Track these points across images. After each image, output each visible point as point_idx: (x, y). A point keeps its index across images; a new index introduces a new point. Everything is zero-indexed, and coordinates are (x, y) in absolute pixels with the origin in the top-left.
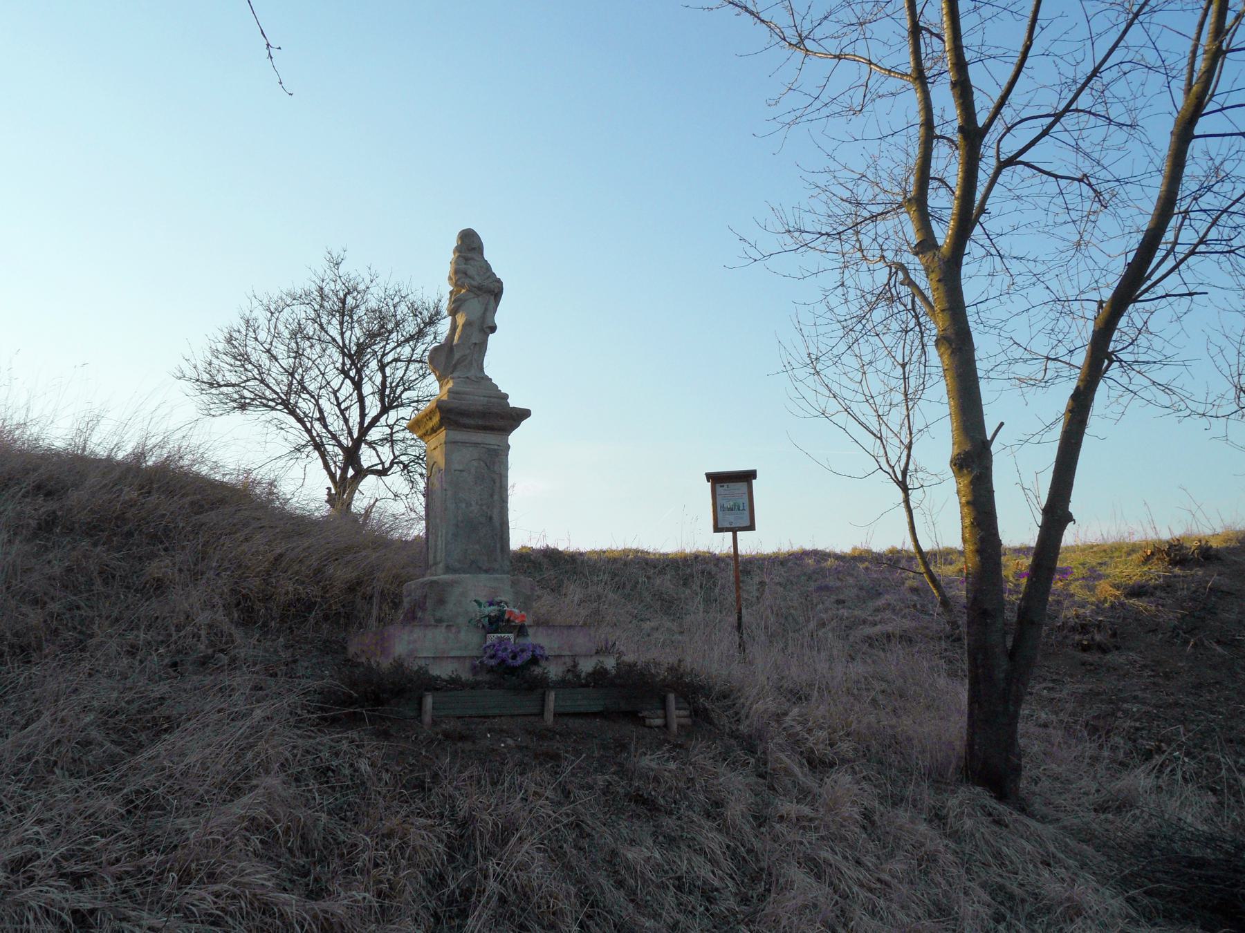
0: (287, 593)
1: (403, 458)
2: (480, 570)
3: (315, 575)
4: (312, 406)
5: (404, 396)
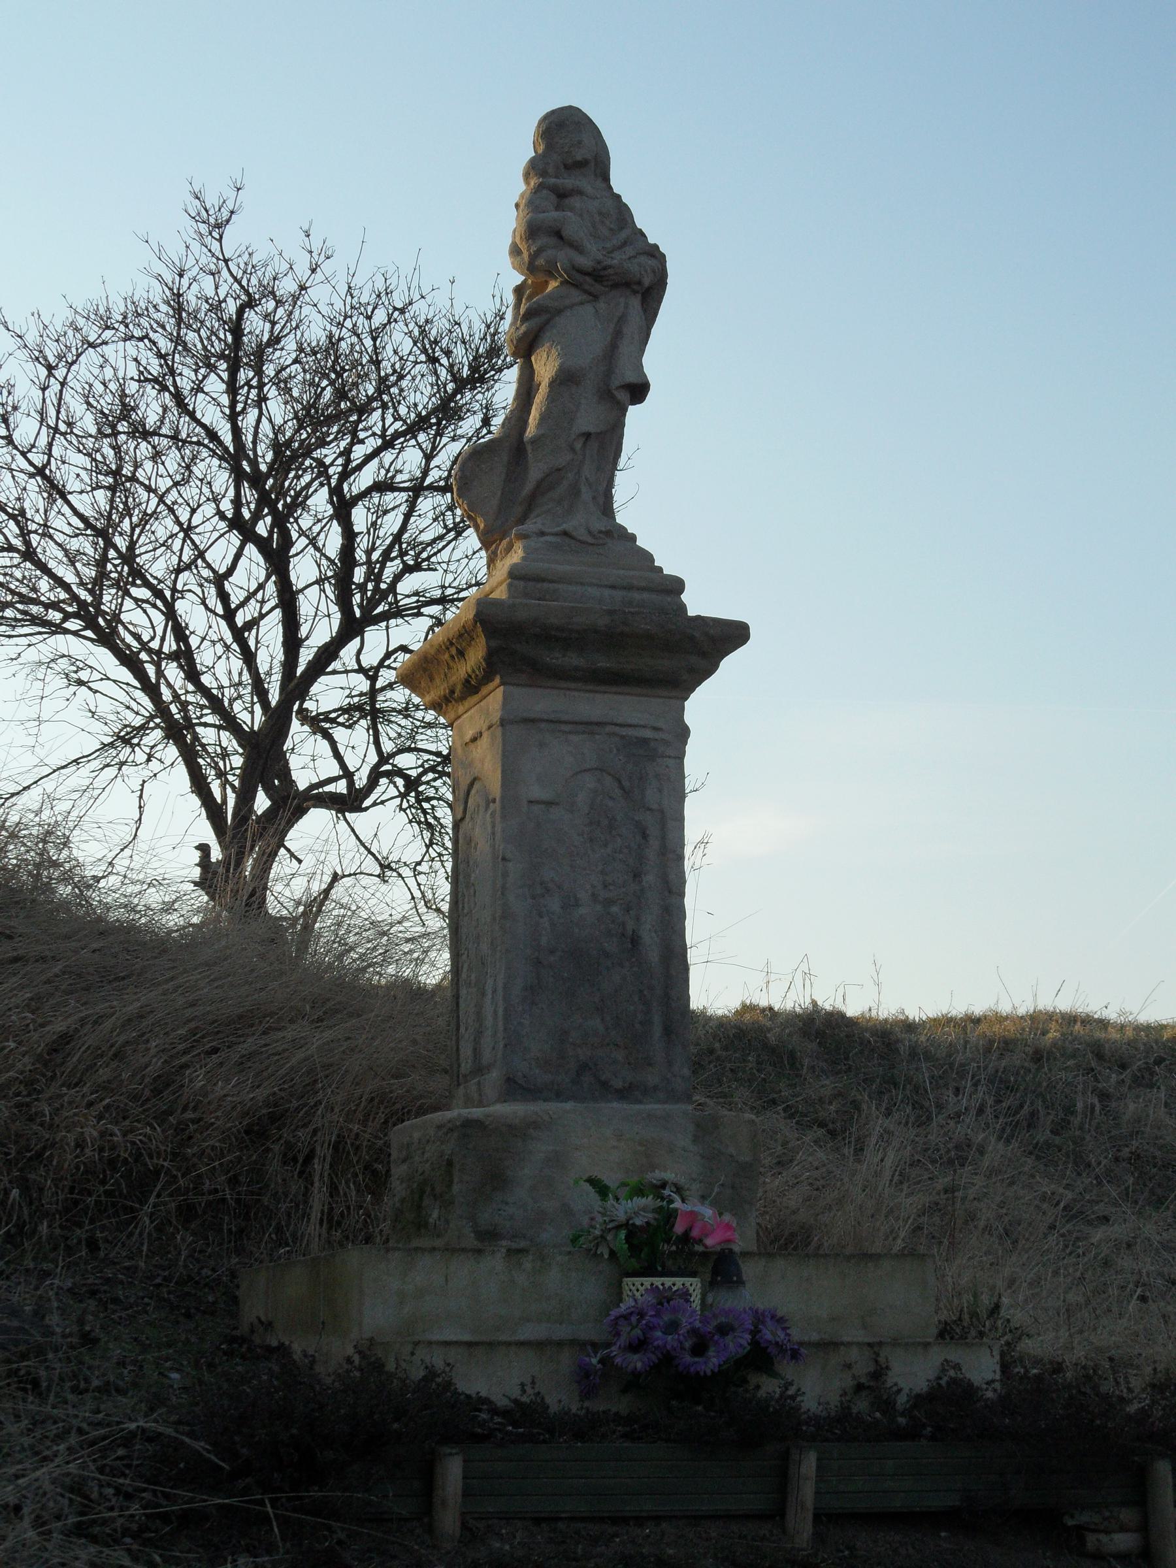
0: (80, 1145)
1: (406, 761)
2: (605, 1090)
3: (157, 1092)
4: (158, 618)
5: (404, 587)
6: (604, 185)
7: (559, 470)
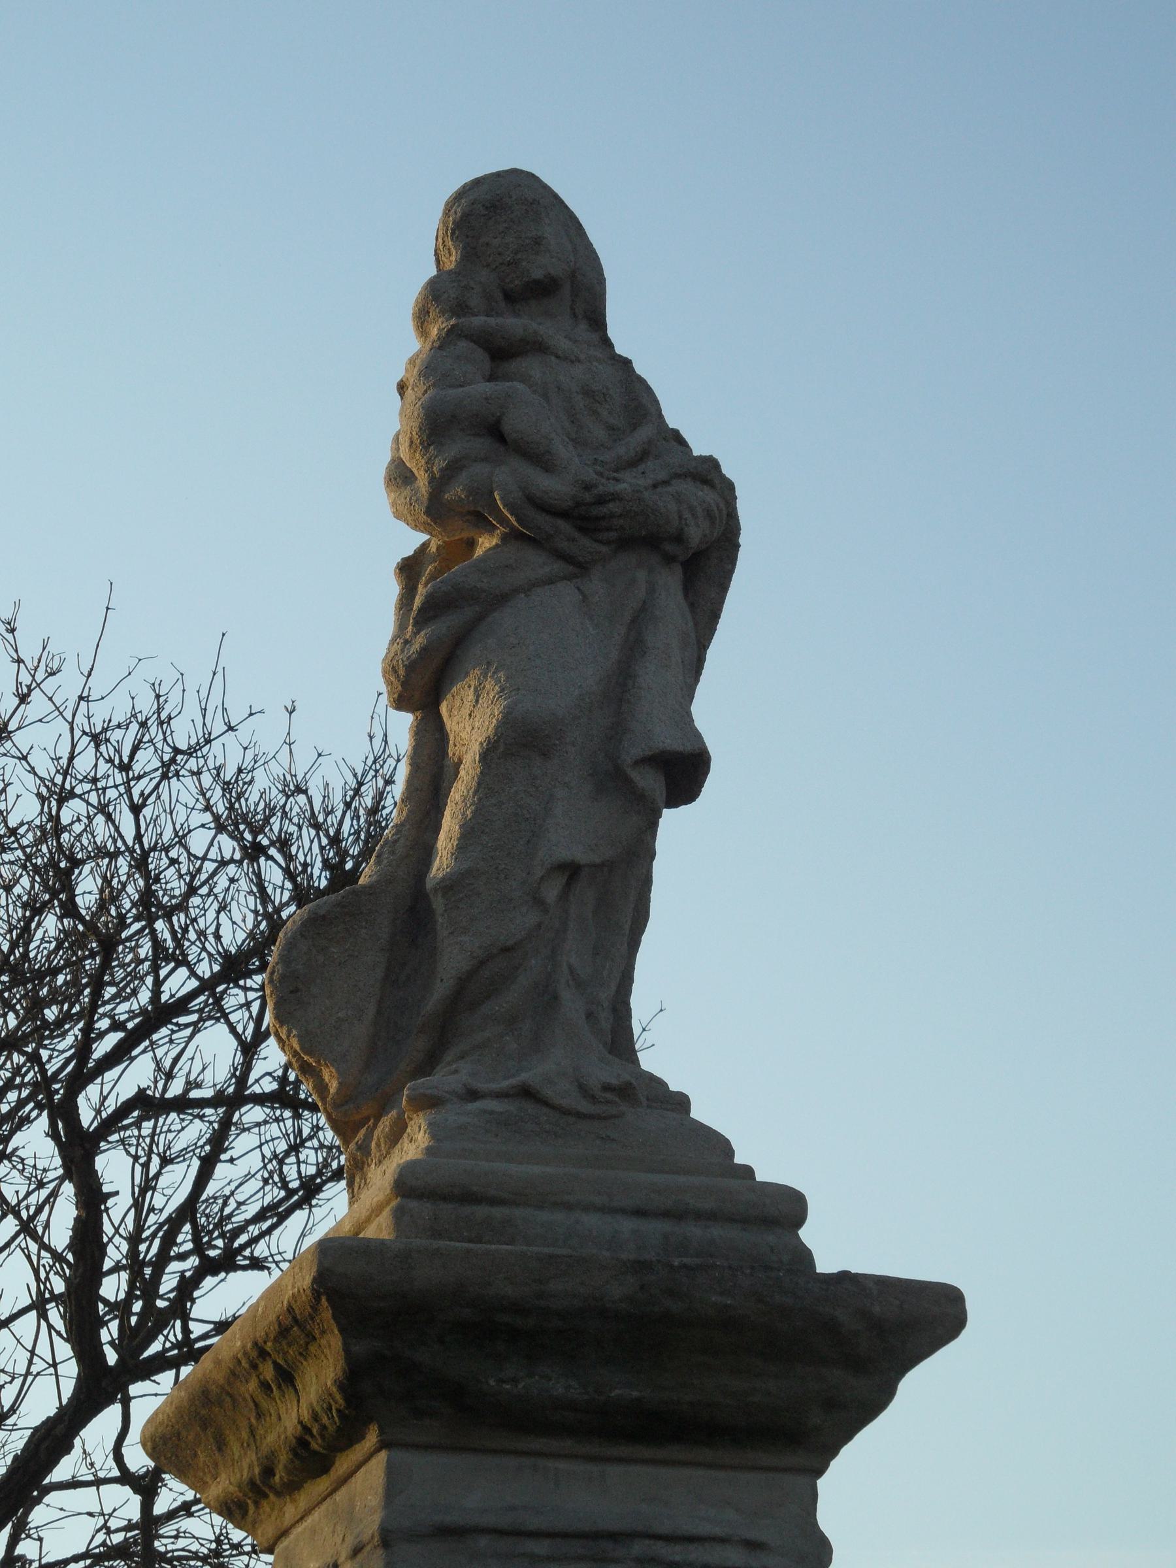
6: (595, 337)
7: (506, 950)
